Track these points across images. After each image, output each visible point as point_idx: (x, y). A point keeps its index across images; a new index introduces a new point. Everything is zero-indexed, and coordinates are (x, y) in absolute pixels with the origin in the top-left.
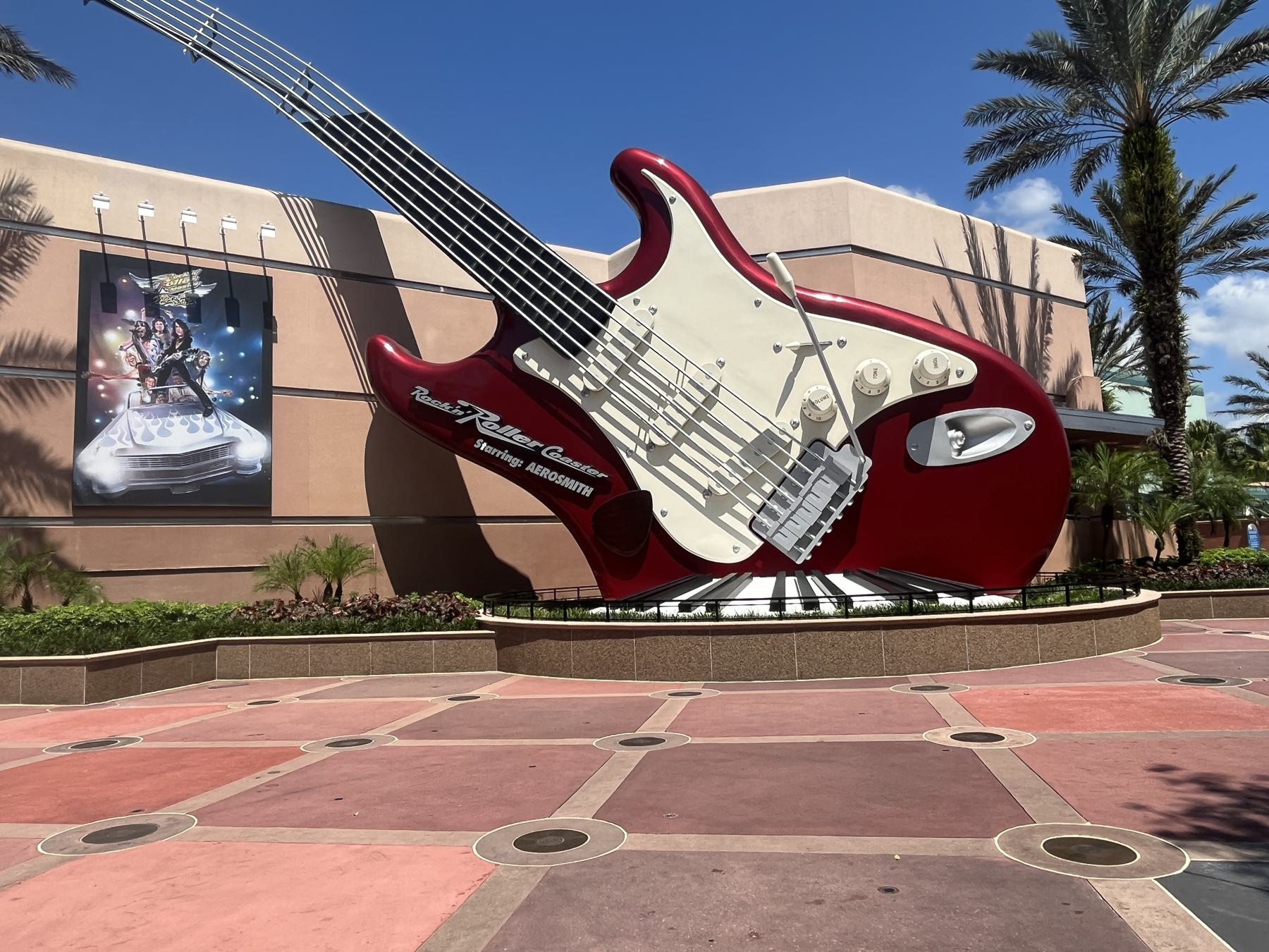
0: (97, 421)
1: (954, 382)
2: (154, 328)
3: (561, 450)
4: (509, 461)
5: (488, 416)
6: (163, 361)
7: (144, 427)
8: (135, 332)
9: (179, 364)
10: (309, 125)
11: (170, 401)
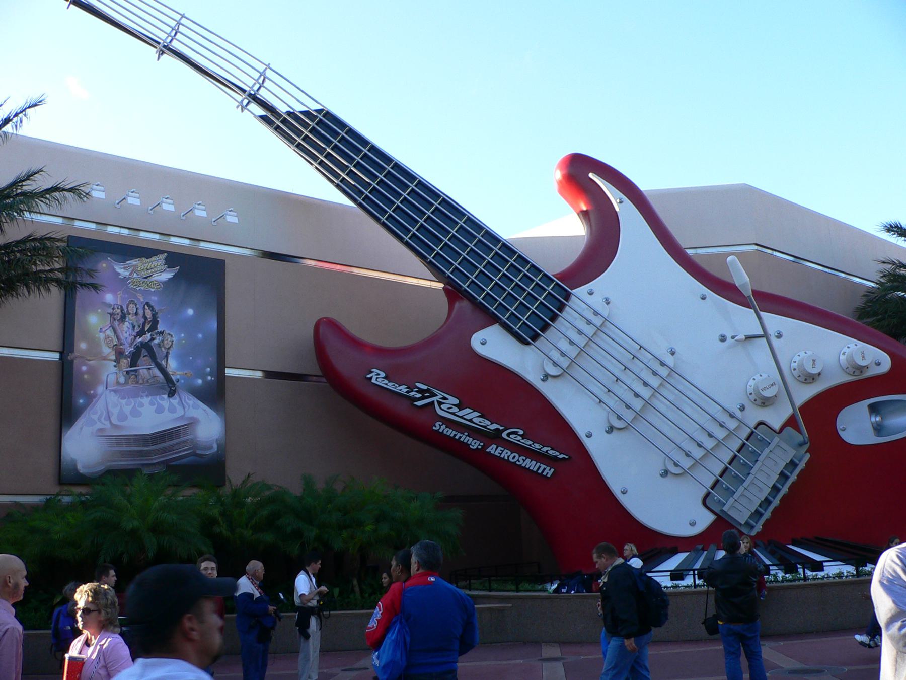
0: (81, 401)
2: (128, 311)
6: (135, 343)
7: (119, 408)
8: (112, 315)
11: (141, 382)
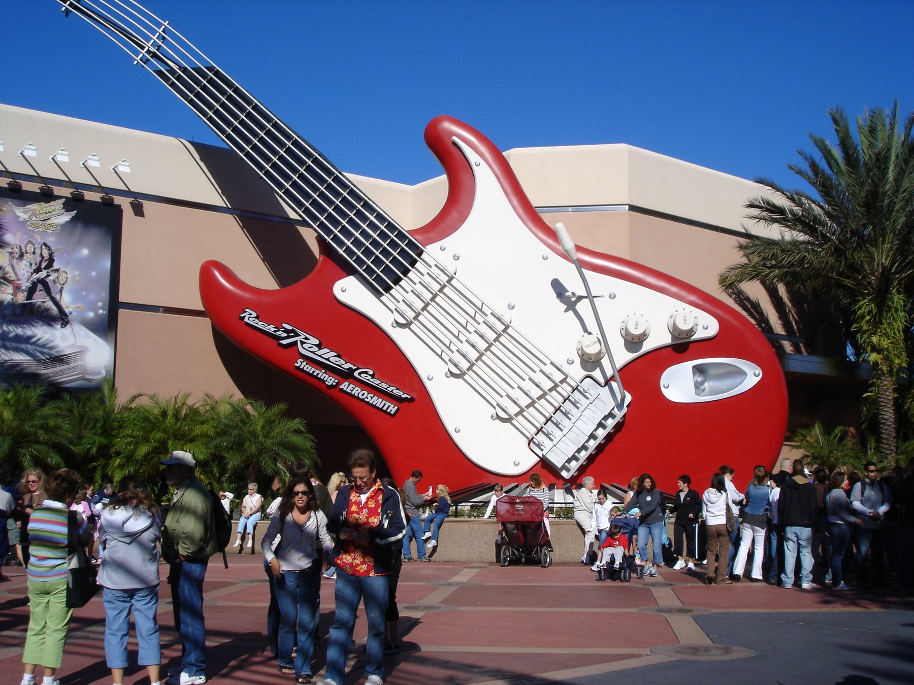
1: (699, 334)
2: (26, 250)
3: (371, 372)
4: (325, 379)
5: (309, 339)
9: (43, 282)
10: (160, 73)
